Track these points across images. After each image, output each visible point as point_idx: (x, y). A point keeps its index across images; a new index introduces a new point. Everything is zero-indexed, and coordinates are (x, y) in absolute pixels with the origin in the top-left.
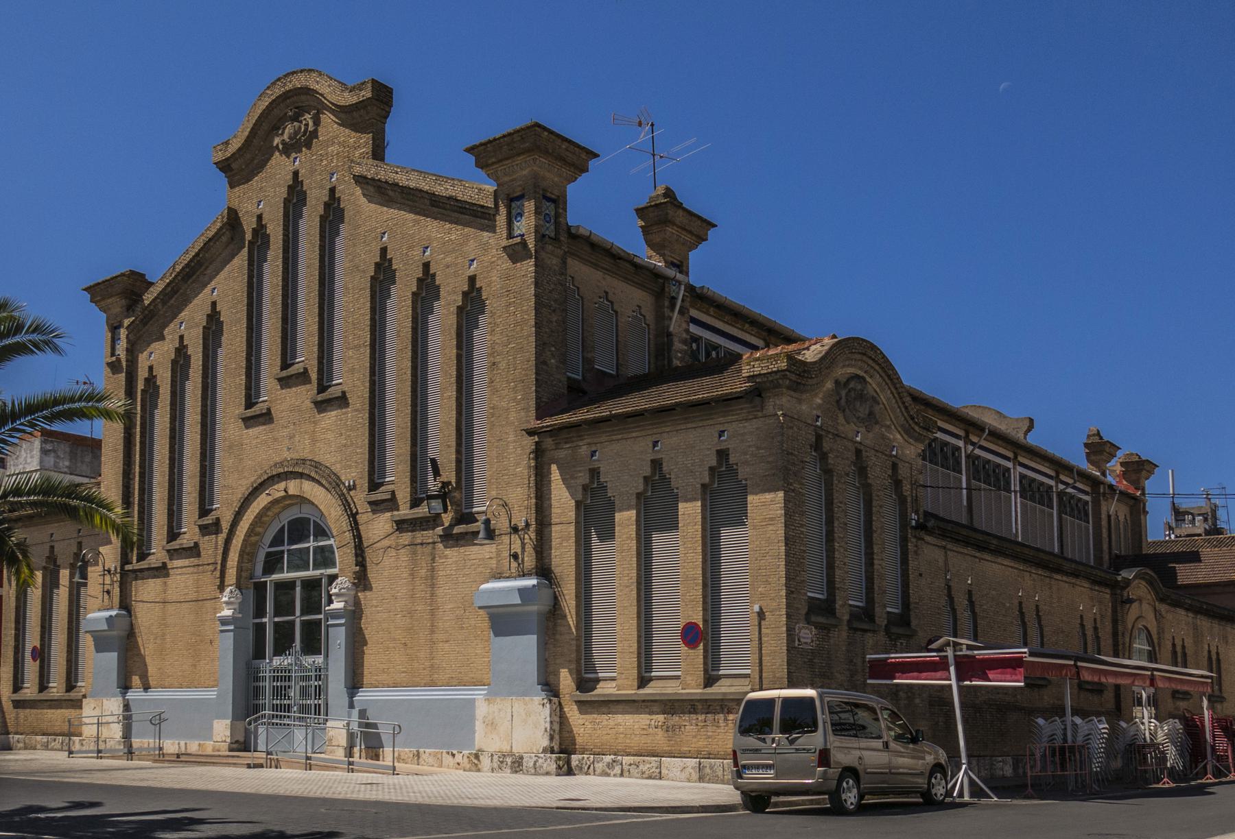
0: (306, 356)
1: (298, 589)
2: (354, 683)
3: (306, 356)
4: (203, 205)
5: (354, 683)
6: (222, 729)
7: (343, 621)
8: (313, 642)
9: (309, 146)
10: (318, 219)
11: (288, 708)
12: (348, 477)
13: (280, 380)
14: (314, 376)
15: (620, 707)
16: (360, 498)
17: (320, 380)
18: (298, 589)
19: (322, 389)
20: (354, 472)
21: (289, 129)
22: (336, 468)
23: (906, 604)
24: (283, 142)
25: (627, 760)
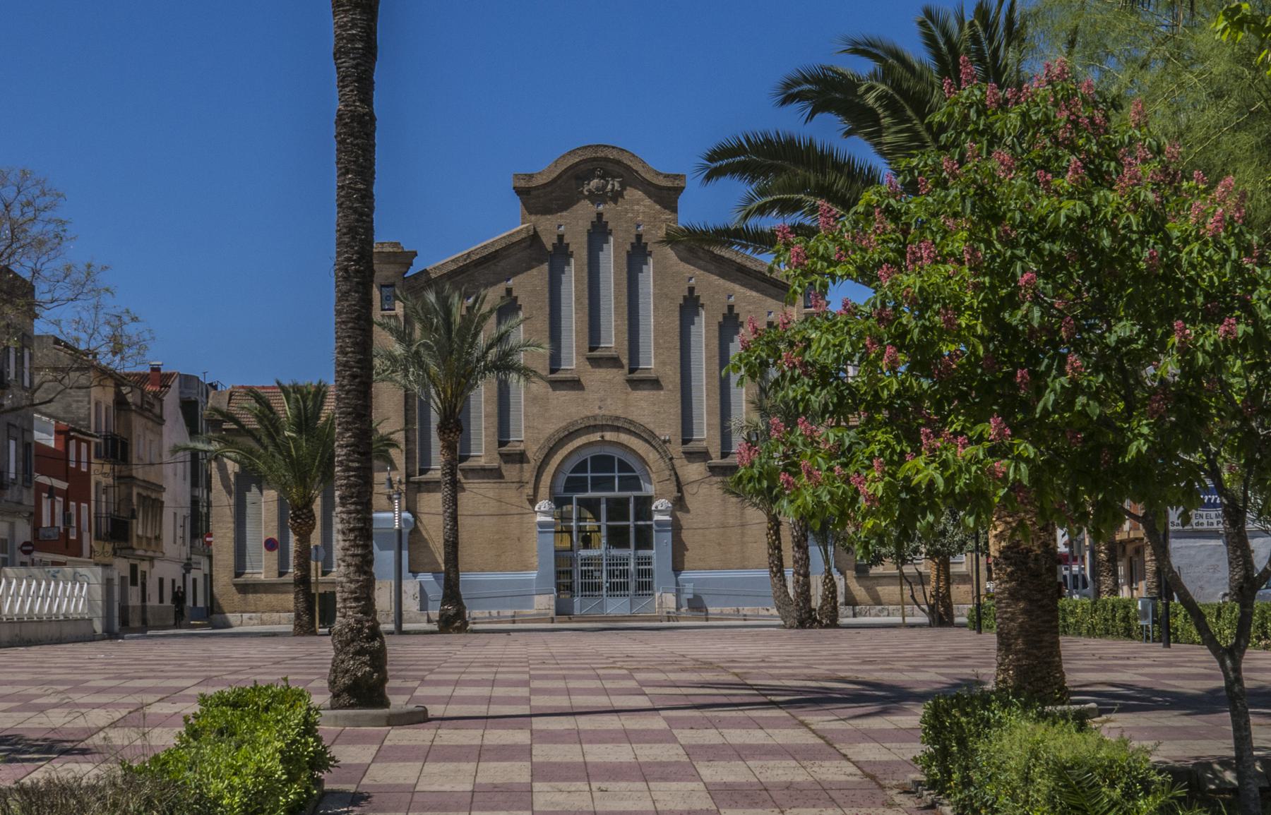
0: (612, 340)
1: (631, 506)
2: (678, 568)
3: (612, 340)
4: (512, 222)
5: (678, 568)
6: (544, 603)
7: (72, 504)
8: (644, 539)
9: (616, 202)
10: (716, 328)
11: (599, 587)
12: (664, 434)
13: (588, 359)
14: (625, 361)
15: (885, 581)
16: (676, 449)
17: (630, 364)
18: (631, 506)
19: (632, 371)
20: (669, 429)
21: (595, 183)
22: (651, 427)
23: (407, 633)
24: (589, 191)
25: (891, 607)
